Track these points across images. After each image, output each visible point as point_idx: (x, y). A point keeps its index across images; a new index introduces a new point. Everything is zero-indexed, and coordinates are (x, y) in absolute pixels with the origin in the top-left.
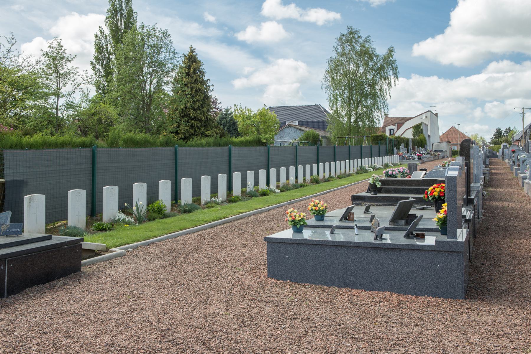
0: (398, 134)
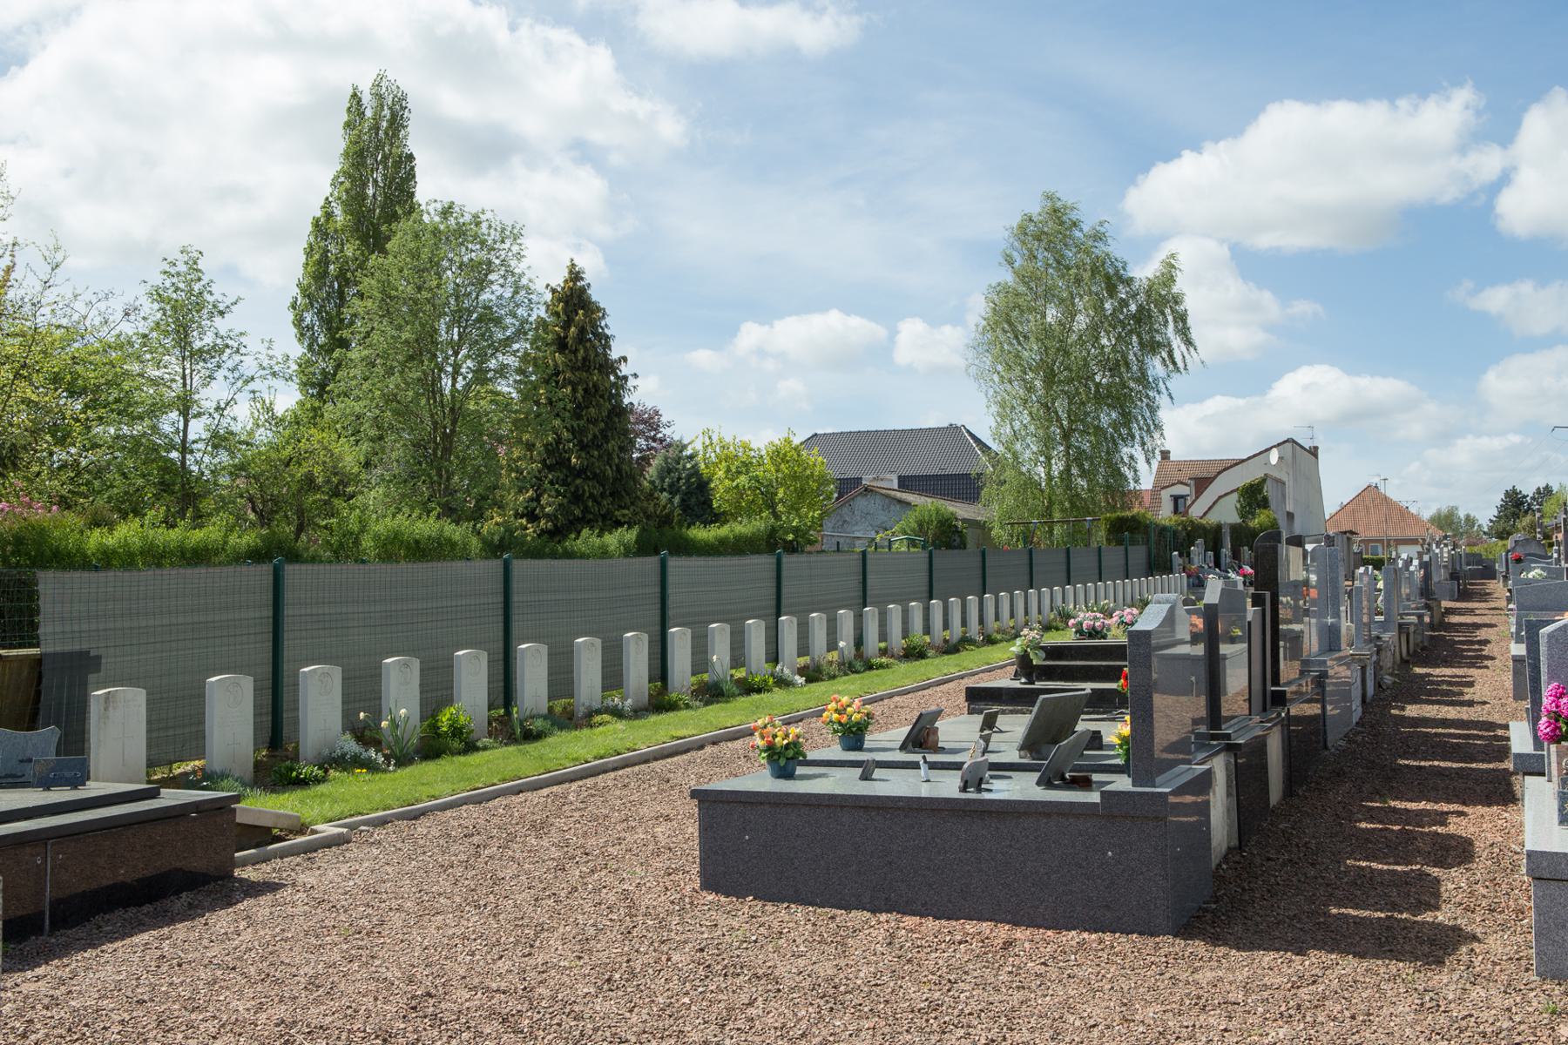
0: (1196, 511)
